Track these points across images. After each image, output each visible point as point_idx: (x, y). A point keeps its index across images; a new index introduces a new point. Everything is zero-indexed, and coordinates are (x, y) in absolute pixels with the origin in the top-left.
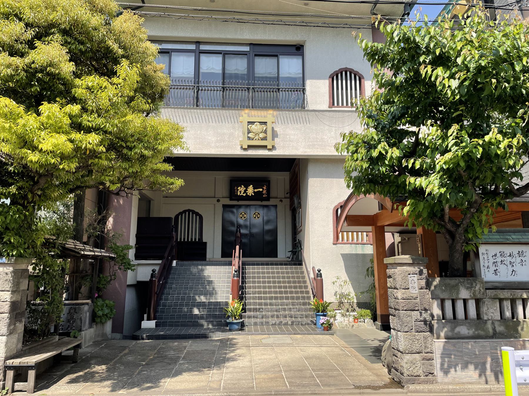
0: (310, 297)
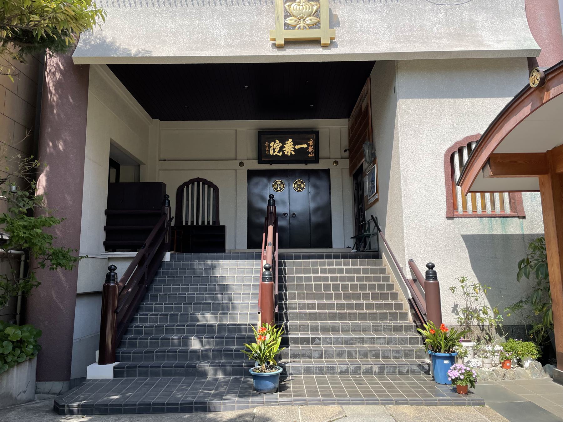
0: (407, 314)
